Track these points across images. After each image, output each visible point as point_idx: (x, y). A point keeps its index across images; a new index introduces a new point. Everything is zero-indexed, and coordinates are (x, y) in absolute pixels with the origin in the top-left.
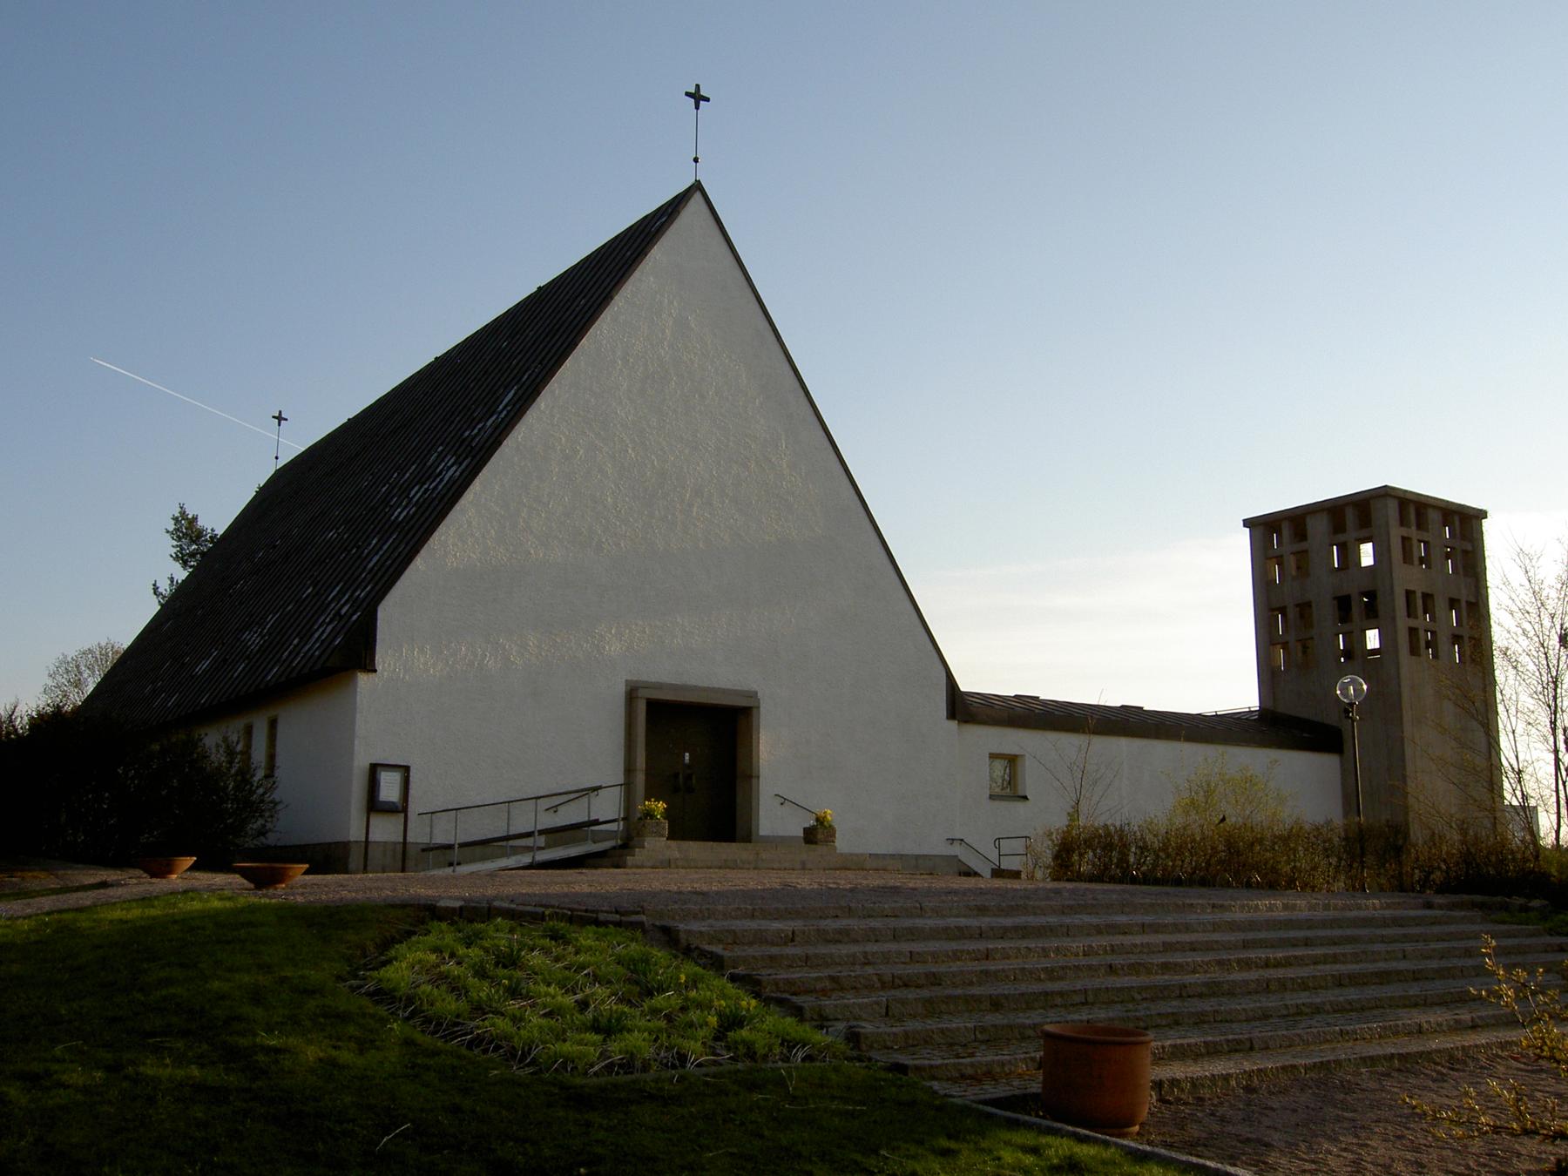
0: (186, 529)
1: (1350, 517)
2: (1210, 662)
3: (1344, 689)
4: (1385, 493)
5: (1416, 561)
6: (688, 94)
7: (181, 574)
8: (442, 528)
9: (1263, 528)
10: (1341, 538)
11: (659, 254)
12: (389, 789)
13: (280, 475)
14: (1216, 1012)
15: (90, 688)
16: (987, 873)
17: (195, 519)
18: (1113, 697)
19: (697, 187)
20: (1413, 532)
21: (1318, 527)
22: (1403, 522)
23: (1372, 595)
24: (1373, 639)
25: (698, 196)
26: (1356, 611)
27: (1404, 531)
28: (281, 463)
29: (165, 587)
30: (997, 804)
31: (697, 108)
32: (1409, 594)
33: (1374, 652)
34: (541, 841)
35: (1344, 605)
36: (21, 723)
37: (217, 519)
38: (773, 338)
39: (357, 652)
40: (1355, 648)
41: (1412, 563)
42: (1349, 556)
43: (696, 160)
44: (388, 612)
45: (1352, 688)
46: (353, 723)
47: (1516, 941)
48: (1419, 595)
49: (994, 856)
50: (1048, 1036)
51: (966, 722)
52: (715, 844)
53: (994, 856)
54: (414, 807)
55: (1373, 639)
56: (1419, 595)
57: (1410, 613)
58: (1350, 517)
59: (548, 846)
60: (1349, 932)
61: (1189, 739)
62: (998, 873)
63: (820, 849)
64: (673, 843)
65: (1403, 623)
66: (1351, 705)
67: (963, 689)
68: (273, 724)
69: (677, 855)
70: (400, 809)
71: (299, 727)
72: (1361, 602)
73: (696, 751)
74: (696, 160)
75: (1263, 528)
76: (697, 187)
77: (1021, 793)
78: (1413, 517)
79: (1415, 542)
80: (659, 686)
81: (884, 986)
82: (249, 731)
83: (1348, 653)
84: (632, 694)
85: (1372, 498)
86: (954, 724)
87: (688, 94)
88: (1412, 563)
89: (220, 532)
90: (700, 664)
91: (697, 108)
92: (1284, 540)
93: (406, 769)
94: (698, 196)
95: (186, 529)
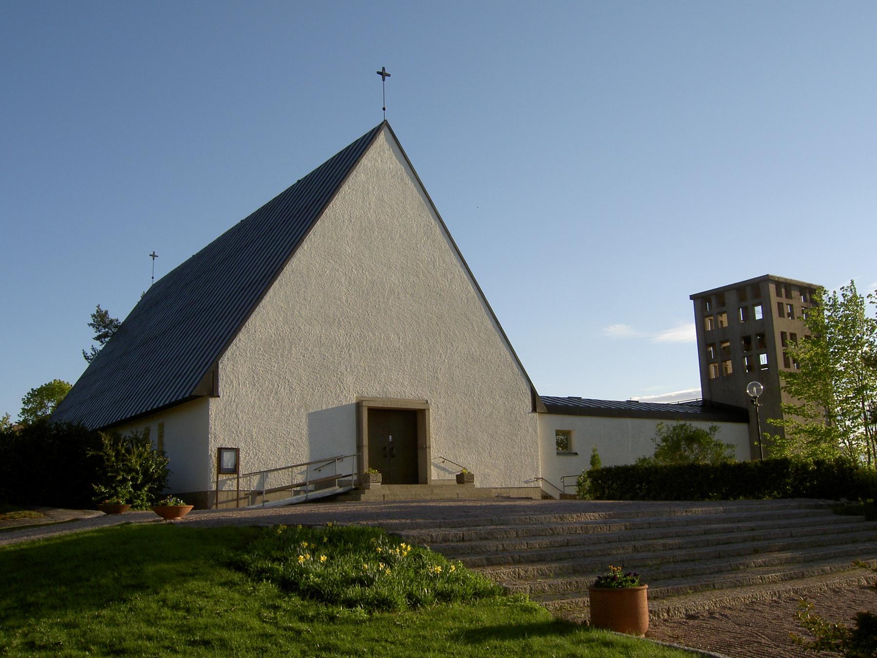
0: (101, 319)
1: (749, 292)
2: (677, 380)
3: (751, 389)
4: (766, 279)
5: (786, 315)
6: (378, 73)
7: (99, 346)
8: (253, 316)
10: (744, 304)
11: (367, 161)
12: (228, 460)
14: (694, 570)
16: (557, 496)
17: (106, 312)
18: (622, 398)
19: (385, 124)
20: (784, 300)
22: (779, 294)
23: (762, 335)
24: (763, 359)
26: (754, 344)
27: (779, 300)
28: (155, 281)
29: (89, 352)
30: (561, 457)
31: (384, 80)
32: (783, 334)
33: (764, 366)
34: (310, 487)
37: (120, 313)
38: (420, 198)
40: (754, 365)
41: (783, 317)
42: (749, 314)
43: (384, 109)
45: (755, 390)
46: (208, 424)
47: (726, 526)
48: (788, 334)
49: (560, 486)
52: (409, 486)
53: (560, 486)
54: (242, 470)
55: (763, 359)
56: (788, 334)
57: (784, 344)
58: (749, 292)
59: (316, 489)
60: (761, 523)
62: (563, 496)
63: (467, 485)
64: (386, 486)
65: (780, 349)
66: (755, 397)
68: (161, 426)
69: (388, 492)
70: (235, 470)
71: (176, 426)
73: (396, 436)
74: (384, 109)
76: (385, 124)
78: (783, 290)
79: (785, 305)
80: (374, 399)
81: (792, 536)
83: (750, 367)
85: (761, 281)
87: (378, 73)
88: (783, 317)
89: (122, 320)
90: (397, 389)
91: (384, 80)
93: (237, 451)
94: (386, 128)
95: (101, 319)
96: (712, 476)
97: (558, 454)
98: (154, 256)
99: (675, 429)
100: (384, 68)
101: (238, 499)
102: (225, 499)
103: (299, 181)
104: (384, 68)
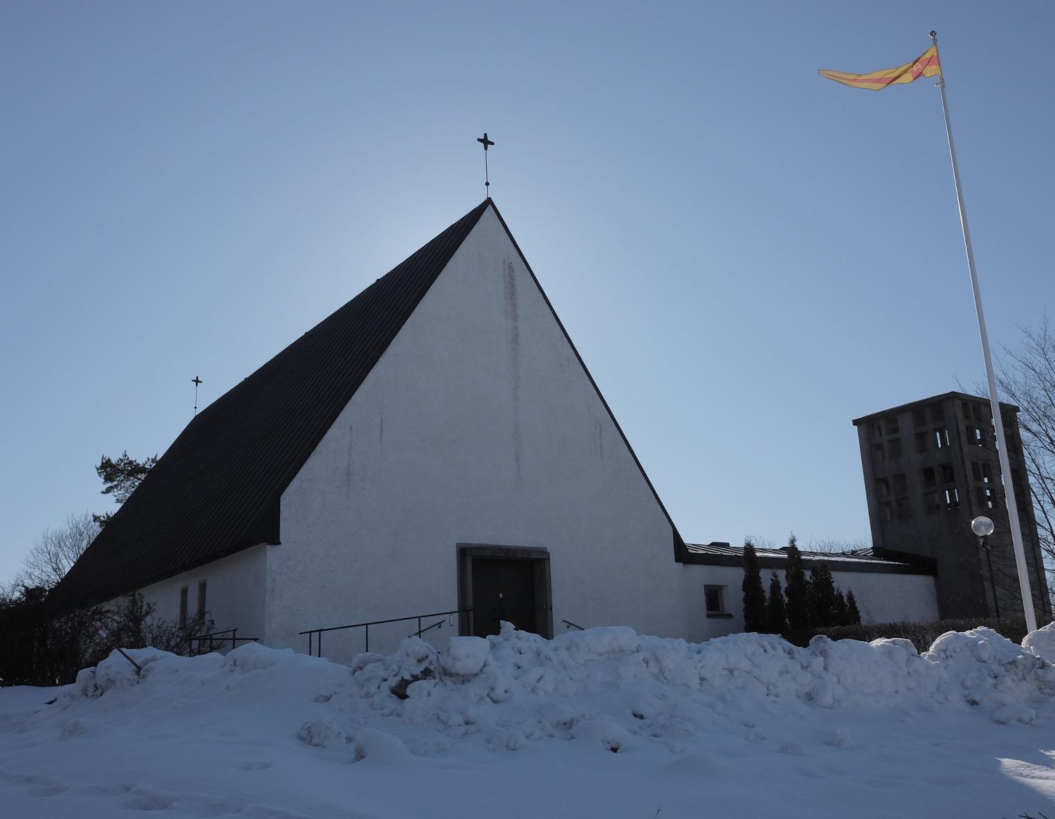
4: (953, 396)
9: (869, 426)
13: (196, 417)
15: (67, 570)
19: (489, 202)
21: (906, 423)
25: (490, 207)
30: (712, 620)
31: (486, 149)
32: (974, 464)
39: (266, 530)
43: (487, 184)
44: (289, 500)
51: (687, 564)
58: (906, 423)
61: (843, 570)
68: (203, 587)
72: (940, 474)
75: (869, 426)
76: (489, 202)
77: (727, 612)
84: (464, 552)
86: (680, 565)
91: (486, 149)
94: (490, 206)
96: (132, 639)
97: (708, 616)
98: (197, 381)
99: (780, 587)
100: (486, 135)
101: (234, 639)
102: (229, 633)
103: (378, 280)
104: (486, 135)
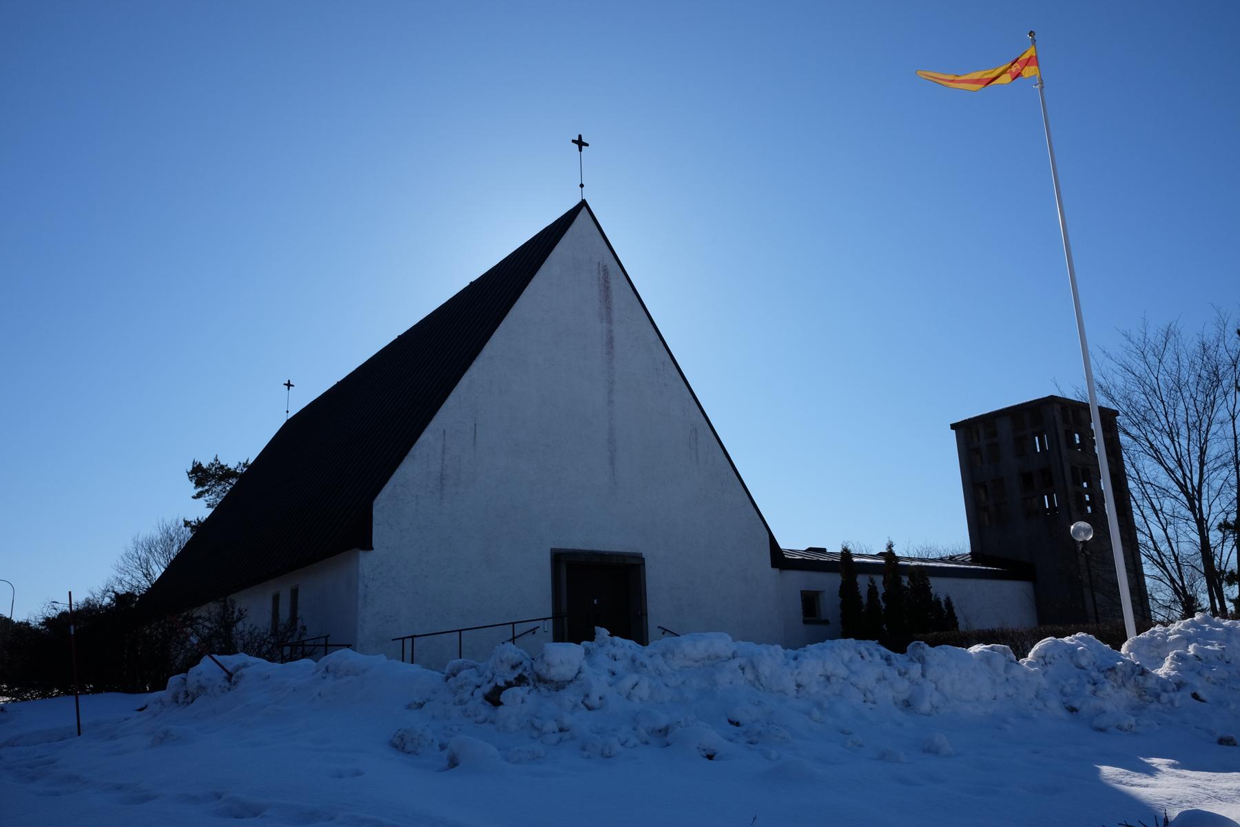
4: (1052, 399)
9: (966, 431)
19: (583, 204)
25: (584, 209)
28: (290, 415)
31: (580, 150)
32: (1073, 469)
35: (1027, 478)
36: (1174, 813)
39: (359, 535)
43: (582, 186)
50: (117, 594)
67: (782, 547)
68: (295, 592)
75: (966, 431)
76: (583, 204)
82: (276, 599)
86: (776, 571)
91: (580, 150)
92: (978, 438)
